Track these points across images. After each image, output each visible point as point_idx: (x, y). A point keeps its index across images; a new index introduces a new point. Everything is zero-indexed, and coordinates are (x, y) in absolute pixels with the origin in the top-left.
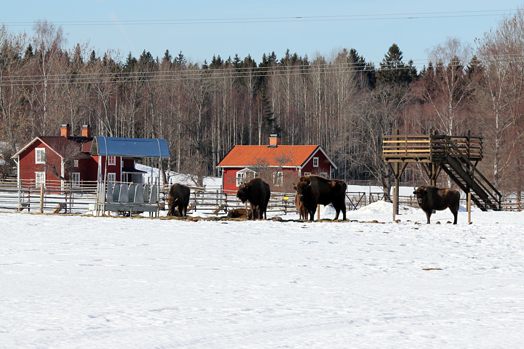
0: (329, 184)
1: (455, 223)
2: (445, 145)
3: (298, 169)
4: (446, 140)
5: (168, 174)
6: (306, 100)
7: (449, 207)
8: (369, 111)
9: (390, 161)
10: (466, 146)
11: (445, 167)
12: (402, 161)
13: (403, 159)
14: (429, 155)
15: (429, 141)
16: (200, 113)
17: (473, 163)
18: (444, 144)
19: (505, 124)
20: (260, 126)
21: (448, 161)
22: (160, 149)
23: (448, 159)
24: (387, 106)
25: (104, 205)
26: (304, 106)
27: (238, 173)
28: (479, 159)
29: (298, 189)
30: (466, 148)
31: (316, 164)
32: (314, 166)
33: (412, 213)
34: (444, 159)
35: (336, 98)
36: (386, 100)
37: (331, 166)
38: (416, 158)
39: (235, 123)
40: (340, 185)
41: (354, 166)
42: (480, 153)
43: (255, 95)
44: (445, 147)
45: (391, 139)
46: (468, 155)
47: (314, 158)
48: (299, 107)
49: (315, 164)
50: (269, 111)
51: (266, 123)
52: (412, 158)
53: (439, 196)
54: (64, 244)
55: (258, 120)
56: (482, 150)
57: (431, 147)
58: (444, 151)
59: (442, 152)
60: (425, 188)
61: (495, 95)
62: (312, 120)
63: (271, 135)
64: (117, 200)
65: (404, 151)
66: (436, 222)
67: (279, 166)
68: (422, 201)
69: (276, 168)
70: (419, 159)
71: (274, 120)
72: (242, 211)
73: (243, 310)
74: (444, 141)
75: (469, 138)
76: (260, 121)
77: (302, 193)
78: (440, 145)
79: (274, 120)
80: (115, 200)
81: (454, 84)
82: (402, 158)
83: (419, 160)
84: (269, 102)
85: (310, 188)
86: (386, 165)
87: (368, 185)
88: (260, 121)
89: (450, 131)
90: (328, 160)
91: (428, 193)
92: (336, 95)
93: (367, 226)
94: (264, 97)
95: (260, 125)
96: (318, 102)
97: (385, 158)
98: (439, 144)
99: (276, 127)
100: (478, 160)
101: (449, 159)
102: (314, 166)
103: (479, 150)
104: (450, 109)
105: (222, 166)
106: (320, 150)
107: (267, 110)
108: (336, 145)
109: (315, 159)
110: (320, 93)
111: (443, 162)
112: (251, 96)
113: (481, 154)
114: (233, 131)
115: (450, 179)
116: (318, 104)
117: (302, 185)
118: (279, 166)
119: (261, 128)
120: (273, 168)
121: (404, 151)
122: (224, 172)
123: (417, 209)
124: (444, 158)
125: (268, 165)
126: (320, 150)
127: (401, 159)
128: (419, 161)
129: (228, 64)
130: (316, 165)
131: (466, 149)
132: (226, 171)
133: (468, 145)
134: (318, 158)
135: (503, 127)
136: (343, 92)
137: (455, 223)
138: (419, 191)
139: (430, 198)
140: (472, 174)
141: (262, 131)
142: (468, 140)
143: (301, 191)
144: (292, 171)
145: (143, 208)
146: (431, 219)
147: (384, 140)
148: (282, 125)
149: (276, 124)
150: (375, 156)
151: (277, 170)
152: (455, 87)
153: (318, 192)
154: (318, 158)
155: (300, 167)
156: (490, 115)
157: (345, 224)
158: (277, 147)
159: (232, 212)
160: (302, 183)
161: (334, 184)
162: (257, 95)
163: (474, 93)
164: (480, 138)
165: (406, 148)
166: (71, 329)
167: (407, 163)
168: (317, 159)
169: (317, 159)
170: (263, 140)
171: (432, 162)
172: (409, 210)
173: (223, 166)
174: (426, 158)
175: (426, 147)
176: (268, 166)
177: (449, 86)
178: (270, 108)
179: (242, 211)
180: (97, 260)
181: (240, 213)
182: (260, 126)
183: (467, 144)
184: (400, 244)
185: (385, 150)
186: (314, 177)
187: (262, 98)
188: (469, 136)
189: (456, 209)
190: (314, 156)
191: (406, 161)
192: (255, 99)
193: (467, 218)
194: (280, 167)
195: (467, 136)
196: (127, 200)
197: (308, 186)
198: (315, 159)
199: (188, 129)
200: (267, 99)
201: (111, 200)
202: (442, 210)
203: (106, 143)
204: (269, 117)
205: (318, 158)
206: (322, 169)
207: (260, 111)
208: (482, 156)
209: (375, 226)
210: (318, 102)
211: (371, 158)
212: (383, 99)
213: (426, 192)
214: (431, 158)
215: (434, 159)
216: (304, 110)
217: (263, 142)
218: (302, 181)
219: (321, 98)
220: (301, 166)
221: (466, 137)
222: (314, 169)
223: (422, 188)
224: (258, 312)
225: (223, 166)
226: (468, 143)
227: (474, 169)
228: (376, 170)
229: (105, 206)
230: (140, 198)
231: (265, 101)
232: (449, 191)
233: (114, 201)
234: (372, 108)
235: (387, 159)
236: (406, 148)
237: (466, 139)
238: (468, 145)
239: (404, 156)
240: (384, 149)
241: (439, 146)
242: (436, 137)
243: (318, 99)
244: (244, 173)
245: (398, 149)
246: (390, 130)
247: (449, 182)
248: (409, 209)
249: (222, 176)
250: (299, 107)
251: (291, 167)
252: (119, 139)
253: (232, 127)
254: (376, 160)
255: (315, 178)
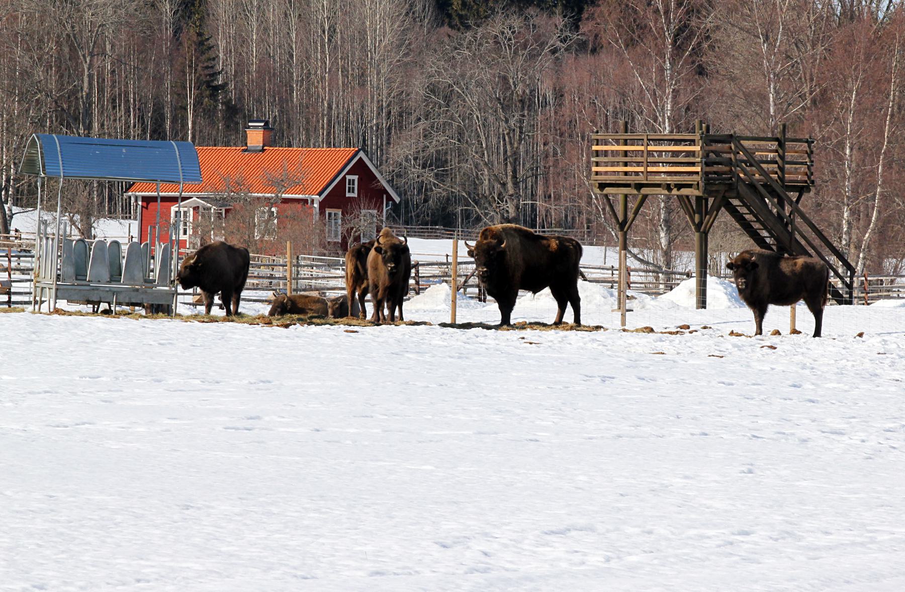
0: (544, 246)
1: (817, 333)
2: (732, 156)
3: (313, 201)
4: (735, 145)
5: (10, 210)
6: (296, 42)
7: (805, 300)
8: (475, 73)
9: (608, 190)
10: (777, 159)
11: (731, 204)
12: (635, 192)
13: (639, 186)
14: (697, 178)
15: (697, 148)
16: (86, 70)
17: (794, 196)
18: (729, 153)
19: (789, 105)
20: (190, 101)
21: (738, 193)
22: (180, 166)
23: (739, 188)
24: (513, 62)
25: (54, 287)
26: (291, 56)
27: (174, 209)
28: (805, 189)
29: (477, 255)
30: (776, 162)
31: (351, 190)
32: (348, 195)
33: (643, 307)
34: (731, 187)
35: (363, 39)
36: (510, 49)
37: (385, 196)
38: (669, 185)
39: (134, 94)
40: (568, 247)
41: (438, 195)
42: (807, 174)
43: (177, 31)
44: (733, 160)
45: (606, 143)
46: (782, 179)
47: (348, 177)
48: (277, 59)
49: (349, 192)
50: (212, 67)
51: (204, 95)
52: (658, 185)
53: (782, 274)
54: (88, 379)
55: (185, 88)
56: (813, 169)
57: (701, 162)
58: (731, 169)
59: (725, 173)
60: (752, 255)
61: (767, 38)
62: (308, 90)
63: (250, 124)
64: (84, 278)
65: (641, 169)
66: (772, 329)
67: (273, 195)
68: (746, 283)
69: (269, 199)
70: (675, 187)
71: (223, 86)
72: (303, 300)
73: (733, 534)
74: (731, 148)
75: (785, 142)
76: (191, 91)
77: (485, 265)
78: (721, 156)
79: (223, 86)
80: (79, 277)
81: (675, 14)
82: (636, 184)
83: (676, 189)
84: (213, 47)
85: (503, 253)
86: (512, 195)
87: (602, 245)
88: (191, 91)
89: (667, 120)
90: (378, 181)
91: (760, 267)
92: (363, 33)
93: (661, 341)
94: (200, 34)
95: (190, 98)
96: (323, 46)
97: (597, 185)
98: (717, 153)
99: (227, 103)
100: (802, 189)
101: (742, 189)
102: (348, 195)
103: (803, 168)
104: (666, 70)
105: (137, 193)
106: (361, 159)
107: (206, 64)
108: (399, 149)
109: (349, 180)
110: (327, 28)
111: (727, 195)
112: (170, 32)
113: (809, 178)
114: (129, 112)
115: (665, 229)
116: (323, 52)
117: (485, 247)
118: (273, 195)
119: (194, 105)
120: (258, 198)
121: (641, 169)
122: (142, 207)
123: (653, 299)
124: (730, 184)
125: (249, 192)
126: (361, 159)
127: (633, 186)
128: (675, 192)
129: (651, 5)
130: (353, 192)
131: (776, 166)
132: (147, 205)
133: (782, 157)
134: (357, 176)
135: (786, 113)
136: (380, 27)
137: (817, 333)
138: (739, 263)
139: (763, 276)
140: (792, 222)
141: (195, 111)
142: (781, 145)
143: (483, 259)
144: (299, 206)
145: (142, 296)
146: (764, 324)
147: (595, 143)
148: (241, 98)
149: (226, 97)
150: (486, 173)
151: (269, 202)
152: (680, 22)
153: (520, 262)
154: (356, 177)
155: (318, 197)
156: (755, 82)
157: (574, 336)
158: (263, 150)
159: (282, 303)
160: (485, 242)
161: (554, 244)
162: (182, 30)
163: (717, 36)
164: (807, 141)
165: (645, 163)
166: (434, 571)
167: (645, 197)
168: (354, 180)
169: (354, 180)
170: (197, 133)
171: (704, 193)
172: (636, 301)
173: (140, 193)
174: (690, 186)
175: (691, 160)
176: (250, 194)
177: (665, 20)
178: (214, 59)
179: (303, 300)
180: (251, 418)
181: (300, 306)
182: (190, 101)
183: (779, 155)
184: (790, 383)
185: (597, 166)
186: (511, 228)
187: (195, 38)
188: (784, 136)
189: (820, 303)
190: (348, 173)
191: (644, 191)
192: (177, 40)
193: (789, 321)
194: (277, 196)
195: (779, 136)
196: (107, 277)
197: (498, 250)
198: (349, 180)
199: (59, 106)
200: (208, 39)
201: (70, 277)
202: (553, 294)
203: (59, 149)
204: (212, 81)
205: (356, 177)
206: (370, 201)
207: (190, 67)
208: (813, 182)
209: (677, 342)
210: (323, 46)
211: (478, 179)
212: (505, 45)
213: (755, 265)
214: (701, 184)
215: (709, 188)
216: (291, 66)
217: (197, 137)
218: (486, 238)
219: (329, 40)
220: (320, 194)
221: (777, 140)
222: (351, 203)
223: (747, 256)
224: (771, 538)
225: (140, 193)
226: (780, 151)
227: (796, 210)
228: (487, 205)
229: (57, 290)
230: (136, 273)
231: (201, 43)
232: (805, 262)
233: (77, 279)
234: (481, 66)
235: (602, 186)
236: (645, 164)
237: (777, 143)
238: (782, 157)
239: (641, 179)
240: (594, 164)
241: (718, 159)
242: (709, 139)
243: (323, 40)
244: (189, 210)
245: (626, 164)
246: (521, 115)
247: (662, 234)
248: (636, 298)
249: (139, 217)
250: (277, 59)
251: (300, 196)
252: (125, 142)
253: (127, 101)
254: (486, 182)
255: (512, 232)
